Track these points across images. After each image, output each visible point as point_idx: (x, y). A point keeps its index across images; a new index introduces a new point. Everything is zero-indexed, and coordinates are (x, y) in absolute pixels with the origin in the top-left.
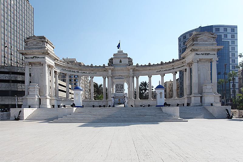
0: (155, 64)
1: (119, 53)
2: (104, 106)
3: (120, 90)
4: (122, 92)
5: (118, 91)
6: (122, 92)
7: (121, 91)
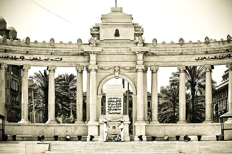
0: (193, 41)
1: (115, 14)
2: (80, 138)
3: (116, 110)
4: (118, 113)
5: (111, 112)
6: (118, 113)
7: (117, 111)
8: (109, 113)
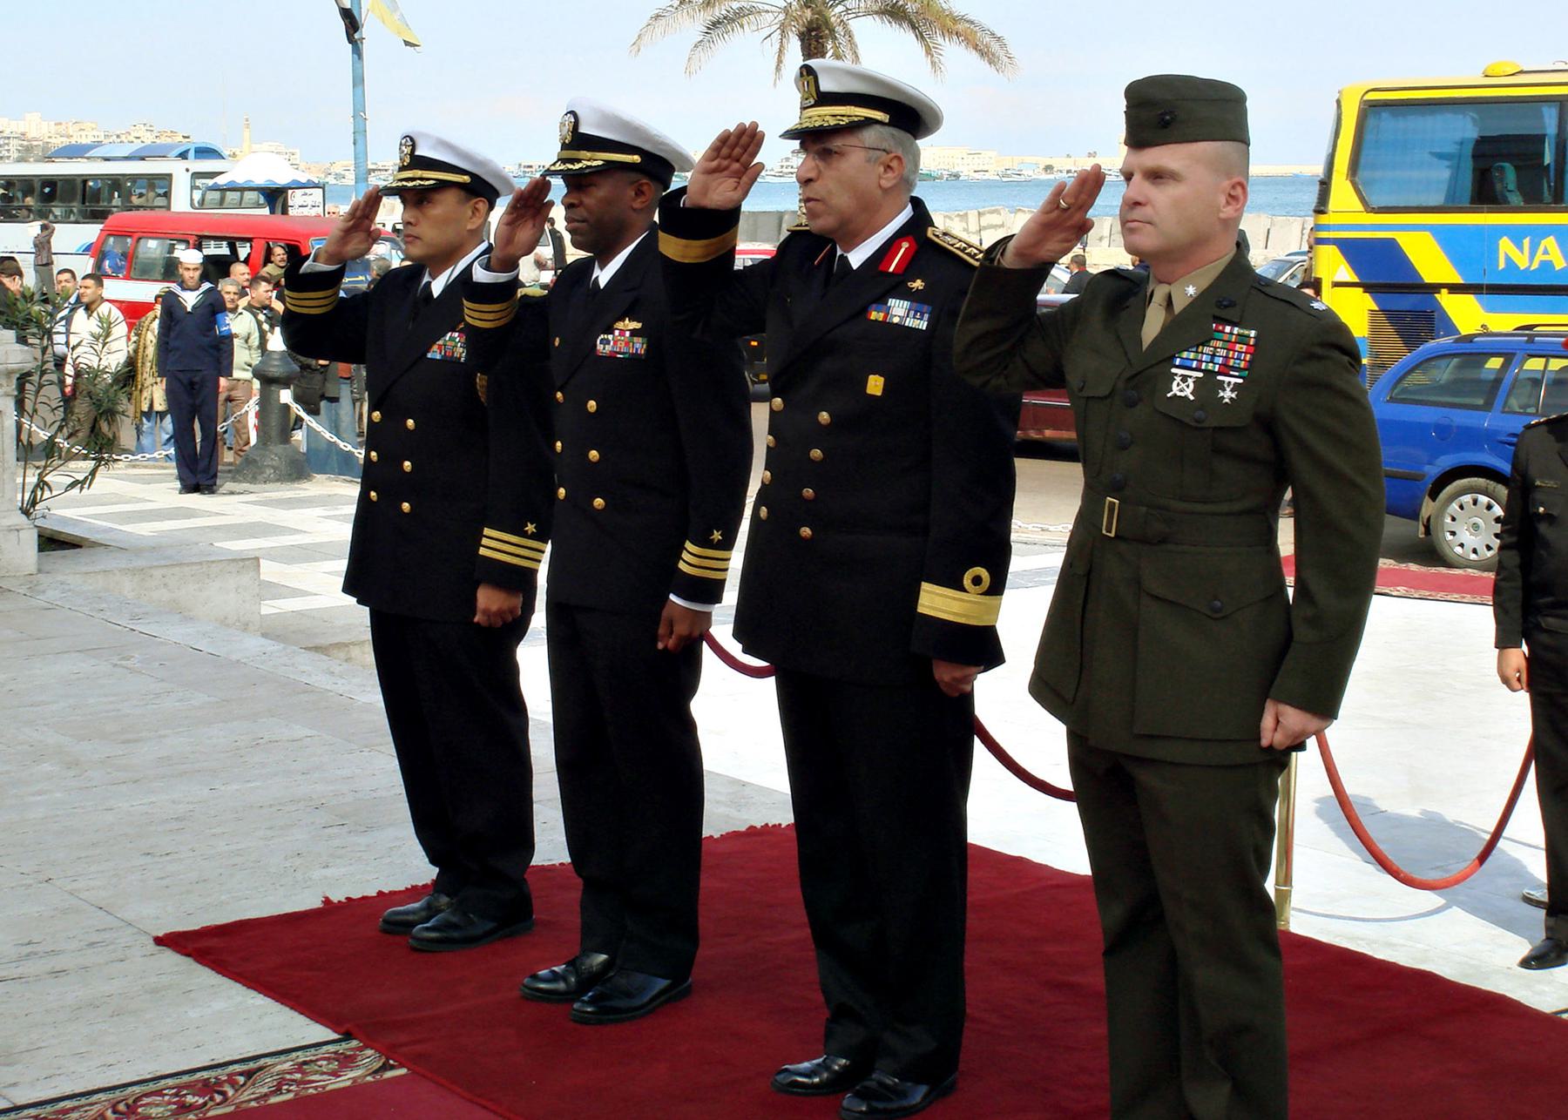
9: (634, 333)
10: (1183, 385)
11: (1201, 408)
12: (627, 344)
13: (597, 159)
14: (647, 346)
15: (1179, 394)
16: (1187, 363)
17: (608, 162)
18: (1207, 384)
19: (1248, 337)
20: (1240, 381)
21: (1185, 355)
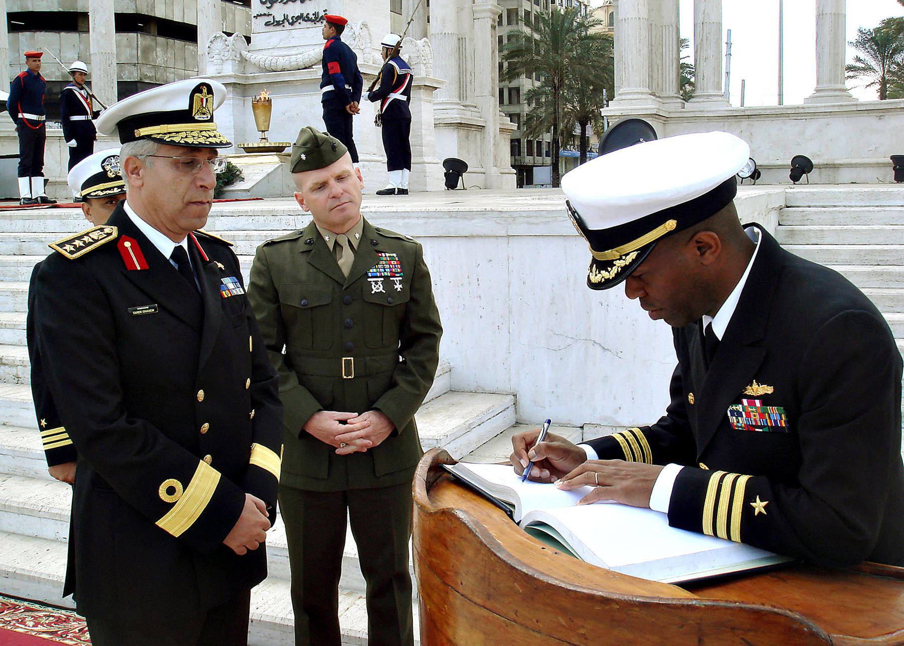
8: (267, 24)
9: (766, 400)
10: (377, 286)
11: (389, 296)
12: (762, 416)
13: (630, 250)
14: (787, 417)
15: (377, 291)
16: (374, 275)
17: (642, 250)
18: (388, 282)
19: (393, 257)
20: (401, 278)
21: (371, 271)
